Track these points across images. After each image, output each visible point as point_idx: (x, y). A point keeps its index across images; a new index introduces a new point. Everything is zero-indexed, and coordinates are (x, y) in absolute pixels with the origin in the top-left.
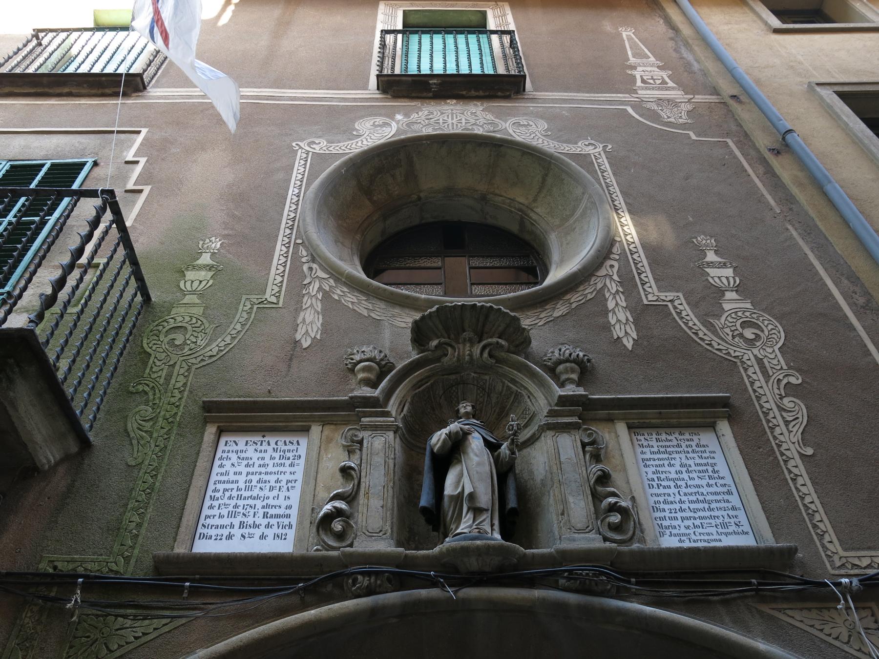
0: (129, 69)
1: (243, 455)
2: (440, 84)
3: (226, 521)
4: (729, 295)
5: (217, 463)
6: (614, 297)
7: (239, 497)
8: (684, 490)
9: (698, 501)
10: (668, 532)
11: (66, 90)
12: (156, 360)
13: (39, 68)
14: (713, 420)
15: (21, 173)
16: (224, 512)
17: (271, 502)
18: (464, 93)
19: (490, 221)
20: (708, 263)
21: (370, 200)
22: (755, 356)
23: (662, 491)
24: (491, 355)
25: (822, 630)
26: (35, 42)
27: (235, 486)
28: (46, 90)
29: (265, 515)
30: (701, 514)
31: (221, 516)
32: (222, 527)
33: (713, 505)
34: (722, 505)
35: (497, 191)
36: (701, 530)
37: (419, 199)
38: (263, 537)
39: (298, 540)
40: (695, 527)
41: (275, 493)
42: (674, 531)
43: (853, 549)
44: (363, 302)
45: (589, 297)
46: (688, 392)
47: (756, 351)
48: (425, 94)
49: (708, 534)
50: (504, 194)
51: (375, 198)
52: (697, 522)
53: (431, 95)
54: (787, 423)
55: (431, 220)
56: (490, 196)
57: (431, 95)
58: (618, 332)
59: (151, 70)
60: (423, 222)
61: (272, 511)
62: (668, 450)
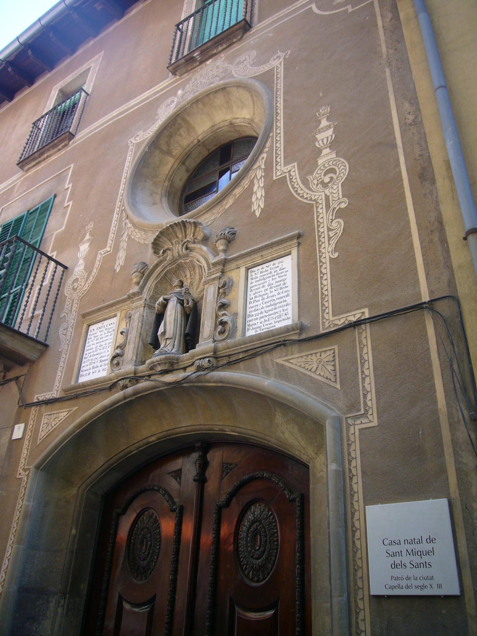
0: (237, 19)
1: (95, 335)
2: (200, 54)
3: (88, 368)
4: (326, 151)
5: (87, 341)
6: (259, 182)
7: (93, 355)
8: (266, 300)
9: (271, 305)
10: (251, 328)
11: (45, 155)
12: (333, 195)
13: (216, 31)
14: (289, 250)
15: (6, 228)
16: (88, 363)
17: (103, 355)
18: (215, 51)
19: (244, 134)
20: (330, 127)
21: (171, 156)
22: (326, 195)
23: (256, 304)
24: (187, 248)
25: (304, 367)
26: (179, 33)
27: (91, 351)
28: (39, 159)
29: (100, 362)
30: (270, 313)
31: (87, 366)
32: (87, 370)
33: (277, 306)
34: (283, 304)
35: (236, 117)
36: (267, 323)
37: (199, 141)
38: (99, 371)
39: (293, 320)
40: (265, 321)
41: (104, 350)
42: (254, 327)
43: (358, 309)
44: (143, 236)
45: (246, 187)
46: (281, 236)
47: (327, 191)
48: (195, 65)
49: (270, 324)
50: (240, 117)
51: (174, 154)
52: (266, 318)
53: (198, 63)
54: (329, 238)
55: (214, 148)
56: (234, 121)
57: (198, 63)
58: (255, 207)
59: (248, 15)
60: (210, 151)
61: (103, 359)
62: (264, 277)
